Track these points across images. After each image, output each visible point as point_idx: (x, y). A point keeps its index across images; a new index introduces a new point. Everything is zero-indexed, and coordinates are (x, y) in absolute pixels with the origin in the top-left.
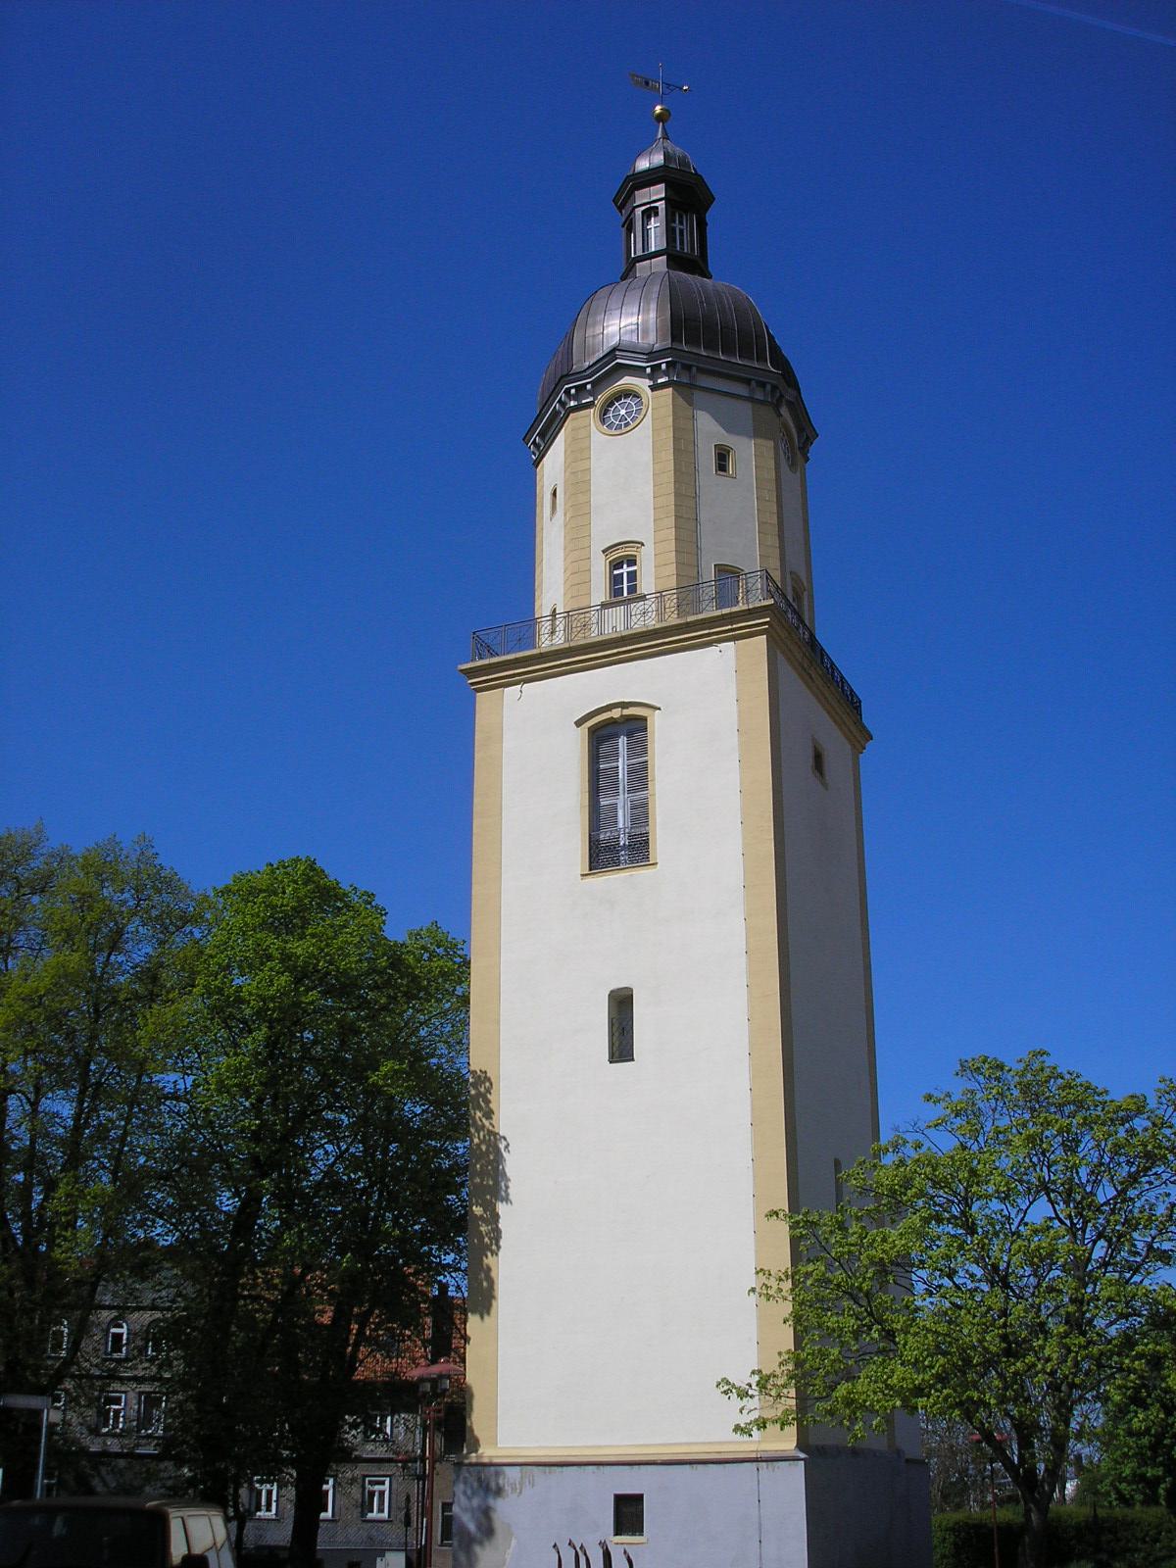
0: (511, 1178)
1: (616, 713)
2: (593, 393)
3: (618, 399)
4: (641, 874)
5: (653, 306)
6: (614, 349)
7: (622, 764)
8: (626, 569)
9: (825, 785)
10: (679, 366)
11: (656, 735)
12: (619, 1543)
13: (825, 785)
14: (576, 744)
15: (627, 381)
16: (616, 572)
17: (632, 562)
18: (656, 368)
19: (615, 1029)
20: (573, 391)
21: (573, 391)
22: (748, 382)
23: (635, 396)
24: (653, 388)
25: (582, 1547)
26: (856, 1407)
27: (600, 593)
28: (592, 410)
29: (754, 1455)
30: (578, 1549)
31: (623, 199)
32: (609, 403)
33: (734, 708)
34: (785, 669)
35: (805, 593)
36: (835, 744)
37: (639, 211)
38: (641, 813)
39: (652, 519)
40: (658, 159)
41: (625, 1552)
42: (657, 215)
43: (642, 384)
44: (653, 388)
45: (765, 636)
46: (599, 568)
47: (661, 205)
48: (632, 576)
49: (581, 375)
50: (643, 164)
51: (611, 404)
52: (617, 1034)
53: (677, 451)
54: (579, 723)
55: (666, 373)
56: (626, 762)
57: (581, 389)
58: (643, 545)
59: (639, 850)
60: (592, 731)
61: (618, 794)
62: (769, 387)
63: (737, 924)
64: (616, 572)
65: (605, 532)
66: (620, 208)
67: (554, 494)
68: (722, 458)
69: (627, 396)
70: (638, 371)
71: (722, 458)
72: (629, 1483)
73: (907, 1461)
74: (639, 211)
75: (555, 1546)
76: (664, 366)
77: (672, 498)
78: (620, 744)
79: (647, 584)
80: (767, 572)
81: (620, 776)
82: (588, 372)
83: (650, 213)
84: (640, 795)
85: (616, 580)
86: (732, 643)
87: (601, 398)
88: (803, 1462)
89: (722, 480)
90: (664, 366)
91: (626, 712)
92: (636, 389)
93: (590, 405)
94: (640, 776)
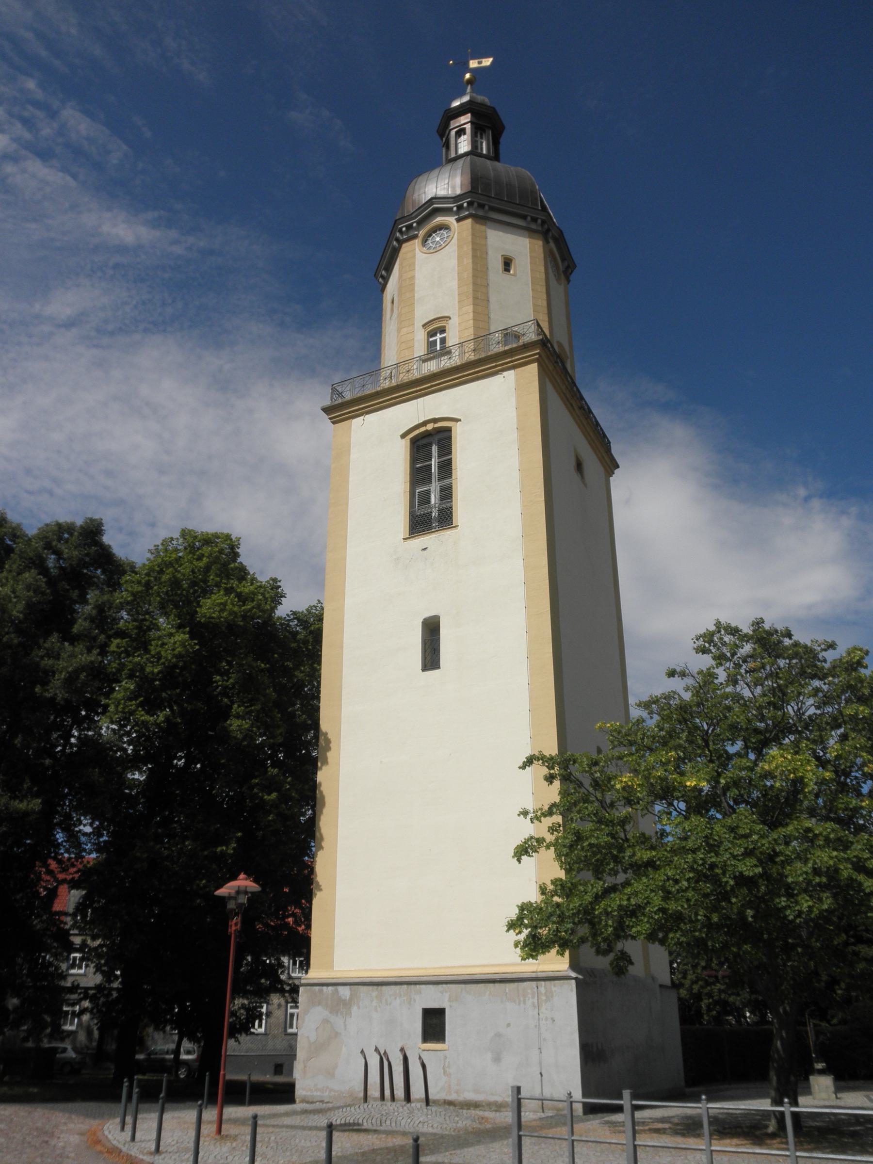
0: (72, 521)
1: (430, 427)
2: (418, 229)
3: (435, 232)
4: (446, 535)
5: (459, 172)
6: (432, 199)
7: (434, 463)
8: (439, 336)
9: (585, 485)
10: (476, 204)
11: (458, 438)
12: (431, 1051)
13: (585, 485)
14: (401, 451)
15: (439, 220)
16: (431, 339)
17: (443, 330)
18: (460, 208)
19: (427, 654)
20: (404, 229)
21: (404, 229)
22: (524, 217)
23: (446, 229)
24: (458, 220)
25: (385, 1053)
26: (685, 748)
27: (420, 349)
28: (417, 241)
29: (534, 975)
30: (382, 1053)
31: (443, 131)
32: (429, 235)
33: (515, 414)
34: (549, 387)
35: (569, 360)
36: (592, 463)
37: (453, 133)
38: (447, 493)
39: (457, 293)
40: (466, 99)
41: (420, 1058)
42: (465, 134)
43: (451, 220)
44: (458, 220)
45: (536, 364)
46: (420, 337)
47: (468, 127)
48: (443, 341)
49: (410, 217)
50: (456, 104)
51: (430, 235)
52: (428, 651)
53: (474, 256)
54: (403, 436)
55: (468, 209)
56: (437, 461)
57: (409, 227)
58: (450, 318)
59: (446, 519)
60: (414, 442)
61: (430, 482)
62: (539, 221)
63: (518, 563)
64: (431, 339)
65: (424, 313)
66: (441, 136)
67: (393, 302)
68: (507, 264)
69: (440, 229)
70: (447, 211)
71: (507, 264)
72: (432, 998)
73: (661, 986)
74: (453, 133)
75: (362, 1052)
76: (465, 205)
77: (471, 286)
78: (433, 449)
79: (453, 339)
80: (537, 322)
81: (433, 471)
82: (413, 215)
83: (461, 132)
84: (447, 482)
85: (431, 345)
86: (513, 371)
87: (422, 233)
88: (573, 982)
89: (506, 276)
90: (465, 205)
91: (436, 425)
92: (446, 223)
93: (415, 237)
94: (446, 468)
